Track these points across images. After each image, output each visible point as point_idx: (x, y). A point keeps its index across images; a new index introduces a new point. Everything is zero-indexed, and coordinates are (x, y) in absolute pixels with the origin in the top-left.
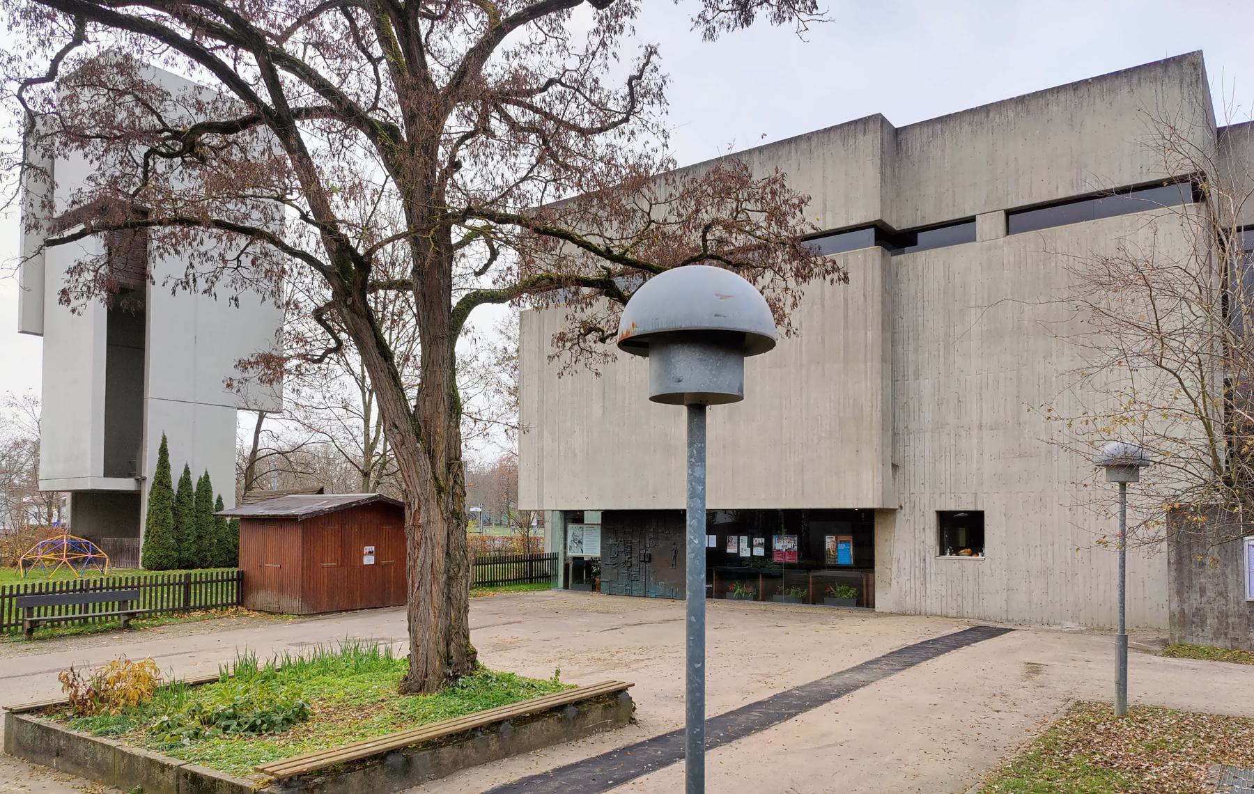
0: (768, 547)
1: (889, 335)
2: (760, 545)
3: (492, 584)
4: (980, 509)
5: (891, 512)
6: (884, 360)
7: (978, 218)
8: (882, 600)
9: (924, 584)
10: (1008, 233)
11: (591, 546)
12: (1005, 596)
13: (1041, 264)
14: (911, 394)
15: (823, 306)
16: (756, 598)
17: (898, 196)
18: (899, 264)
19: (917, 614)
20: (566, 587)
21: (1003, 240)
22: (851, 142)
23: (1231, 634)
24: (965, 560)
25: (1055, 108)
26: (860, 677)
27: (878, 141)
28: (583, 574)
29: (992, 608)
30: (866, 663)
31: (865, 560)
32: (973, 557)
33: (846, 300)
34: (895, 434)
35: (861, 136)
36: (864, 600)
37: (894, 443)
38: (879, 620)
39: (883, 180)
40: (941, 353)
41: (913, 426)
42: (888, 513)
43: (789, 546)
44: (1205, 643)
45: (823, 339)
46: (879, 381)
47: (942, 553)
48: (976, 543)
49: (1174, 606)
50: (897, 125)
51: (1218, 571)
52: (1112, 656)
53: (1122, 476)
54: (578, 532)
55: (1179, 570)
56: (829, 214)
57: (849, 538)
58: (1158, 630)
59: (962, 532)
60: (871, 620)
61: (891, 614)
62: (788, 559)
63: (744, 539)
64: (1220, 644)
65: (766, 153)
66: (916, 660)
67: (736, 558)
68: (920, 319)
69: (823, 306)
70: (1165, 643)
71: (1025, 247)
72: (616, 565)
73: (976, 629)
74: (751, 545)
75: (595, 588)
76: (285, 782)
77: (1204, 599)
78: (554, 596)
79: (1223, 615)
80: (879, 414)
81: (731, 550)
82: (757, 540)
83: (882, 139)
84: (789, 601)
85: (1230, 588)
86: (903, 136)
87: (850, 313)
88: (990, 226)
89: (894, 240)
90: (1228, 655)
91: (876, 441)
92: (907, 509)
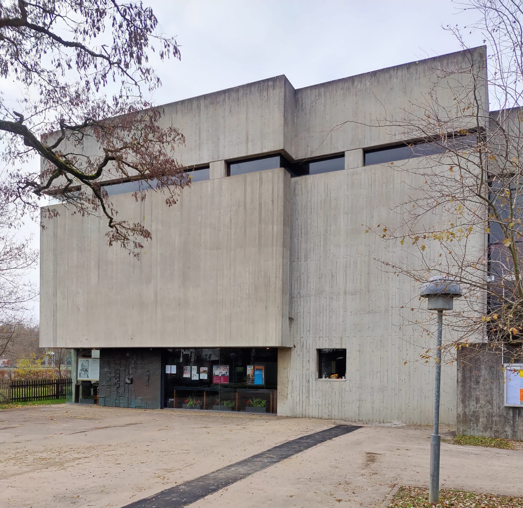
0: (210, 373)
1: (288, 230)
2: (204, 372)
3: (25, 400)
4: (344, 347)
5: (289, 349)
6: (284, 246)
7: (346, 153)
8: (282, 408)
9: (308, 397)
10: (364, 164)
11: (93, 373)
12: (358, 405)
13: (384, 185)
14: (303, 271)
15: (245, 208)
16: (202, 408)
17: (296, 136)
18: (296, 183)
19: (303, 417)
20: (77, 401)
21: (361, 169)
22: (265, 94)
23: (494, 428)
24: (334, 382)
25: (395, 80)
26: (242, 470)
27: (282, 95)
28: (88, 393)
29: (349, 413)
30: (253, 457)
31: (271, 382)
32: (339, 380)
33: (260, 204)
34: (291, 297)
35: (271, 90)
36: (271, 409)
37: (291, 303)
38: (277, 422)
39: (285, 119)
40: (322, 244)
41: (303, 292)
42: (287, 350)
43: (224, 372)
44: (478, 434)
45: (245, 230)
46: (281, 260)
47: (320, 377)
48: (341, 372)
49: (460, 410)
50: (297, 86)
51: (487, 387)
52: (428, 447)
53: (440, 303)
54: (85, 364)
55: (464, 386)
56: (250, 144)
57: (262, 367)
58: (449, 425)
59: (332, 362)
60: (272, 422)
61: (287, 417)
62: (222, 382)
63: (195, 368)
64: (487, 434)
65: (209, 100)
66: (291, 452)
67: (189, 382)
68: (309, 220)
69: (245, 208)
70: (453, 434)
71: (374, 174)
72: (109, 386)
73: (338, 427)
74: (199, 372)
75: (96, 402)
76: (59, 498)
77: (479, 405)
78: (67, 408)
79: (490, 415)
80: (281, 283)
81: (186, 375)
82: (202, 369)
83: (285, 93)
84: (223, 409)
85: (494, 398)
86: (299, 95)
87: (263, 214)
88: (353, 159)
89: (296, 167)
90: (494, 442)
91: (279, 301)
92: (298, 347)
